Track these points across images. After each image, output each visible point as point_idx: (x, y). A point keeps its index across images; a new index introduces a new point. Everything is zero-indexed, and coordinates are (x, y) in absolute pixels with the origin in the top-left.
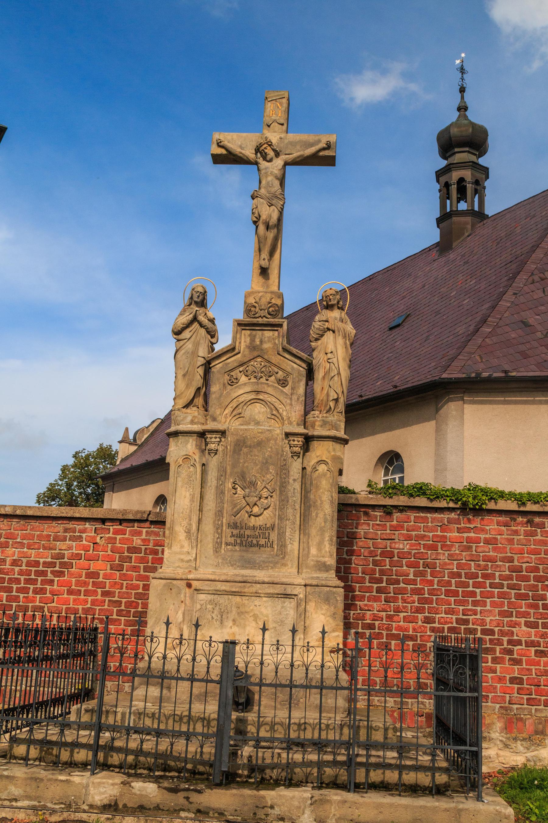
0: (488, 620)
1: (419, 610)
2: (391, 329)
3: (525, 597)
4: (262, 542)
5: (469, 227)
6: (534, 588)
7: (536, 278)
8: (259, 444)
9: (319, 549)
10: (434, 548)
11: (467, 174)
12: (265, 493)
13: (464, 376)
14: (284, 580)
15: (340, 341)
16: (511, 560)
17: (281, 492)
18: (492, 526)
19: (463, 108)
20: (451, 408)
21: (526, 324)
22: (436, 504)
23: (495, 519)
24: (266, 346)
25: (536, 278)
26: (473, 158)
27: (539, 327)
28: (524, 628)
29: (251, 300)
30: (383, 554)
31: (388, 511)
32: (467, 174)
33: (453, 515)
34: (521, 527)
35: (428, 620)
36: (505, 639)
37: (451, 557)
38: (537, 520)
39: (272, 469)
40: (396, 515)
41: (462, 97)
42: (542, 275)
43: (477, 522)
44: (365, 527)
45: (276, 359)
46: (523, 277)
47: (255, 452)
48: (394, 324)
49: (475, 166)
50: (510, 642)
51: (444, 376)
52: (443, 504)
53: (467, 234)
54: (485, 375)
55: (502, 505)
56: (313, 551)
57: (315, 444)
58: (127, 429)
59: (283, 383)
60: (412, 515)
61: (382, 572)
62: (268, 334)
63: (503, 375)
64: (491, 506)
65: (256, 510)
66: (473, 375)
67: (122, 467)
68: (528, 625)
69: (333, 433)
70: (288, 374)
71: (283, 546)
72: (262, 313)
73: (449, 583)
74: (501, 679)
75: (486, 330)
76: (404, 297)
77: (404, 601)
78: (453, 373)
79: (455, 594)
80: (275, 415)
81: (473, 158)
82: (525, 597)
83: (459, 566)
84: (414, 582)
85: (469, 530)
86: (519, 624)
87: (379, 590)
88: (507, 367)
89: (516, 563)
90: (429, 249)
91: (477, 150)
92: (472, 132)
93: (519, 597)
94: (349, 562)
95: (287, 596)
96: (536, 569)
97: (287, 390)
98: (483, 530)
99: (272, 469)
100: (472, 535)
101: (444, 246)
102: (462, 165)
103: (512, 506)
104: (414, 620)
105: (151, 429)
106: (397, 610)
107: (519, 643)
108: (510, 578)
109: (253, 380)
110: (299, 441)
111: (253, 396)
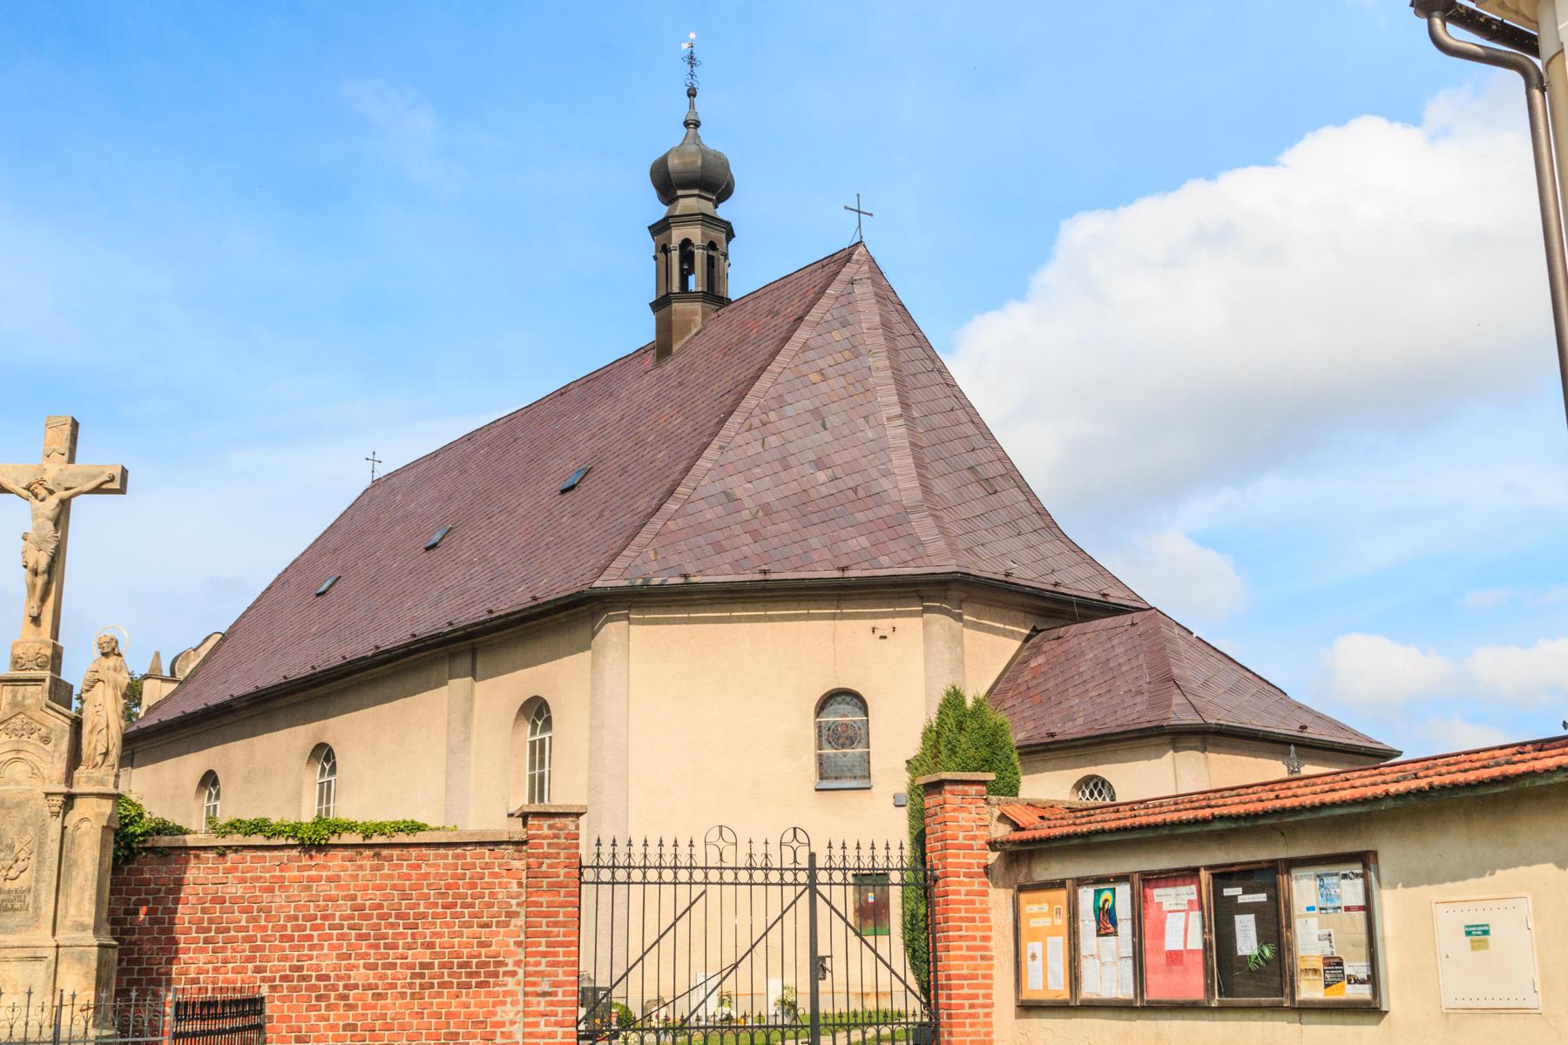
0: (324, 964)
1: (249, 960)
2: (563, 492)
3: (366, 937)
4: (17, 905)
5: (699, 319)
6: (377, 927)
7: (756, 422)
8: (19, 805)
9: (79, 909)
10: (270, 890)
11: (695, 233)
12: (22, 856)
13: (626, 583)
14: (36, 943)
15: (110, 692)
16: (354, 898)
17: (39, 853)
18: (336, 861)
19: (692, 124)
20: (612, 632)
21: (729, 497)
22: (274, 842)
23: (341, 853)
24: (28, 702)
25: (756, 422)
26: (707, 207)
27: (748, 503)
28: (362, 970)
29: (19, 651)
30: (213, 901)
31: (222, 852)
32: (695, 233)
33: (294, 853)
34: (367, 860)
35: (258, 970)
36: (341, 984)
37: (289, 900)
38: (385, 852)
39: (31, 830)
40: (231, 856)
41: (692, 105)
42: (764, 417)
43: (320, 858)
44: (195, 871)
45: (38, 715)
46: (735, 420)
47: (14, 812)
48: (567, 485)
49: (708, 220)
50: (346, 987)
51: (598, 584)
52: (281, 841)
53: (694, 331)
54: (656, 581)
55: (347, 838)
56: (72, 911)
57: (78, 801)
58: (157, 655)
59: (46, 740)
60: (248, 855)
61: (211, 921)
62: (31, 689)
63: (681, 580)
64: (334, 840)
65: (12, 873)
66: (639, 582)
67: (143, 725)
68: (368, 967)
69: (103, 790)
70: (51, 730)
71: (37, 909)
72: (29, 665)
73: (284, 928)
74: (333, 1028)
75: (671, 506)
76: (594, 435)
77: (234, 951)
78: (611, 580)
79: (291, 938)
80: (35, 773)
81: (707, 207)
82: (366, 937)
83: (296, 909)
84: (246, 929)
85: (310, 868)
86: (357, 967)
87: (206, 941)
88: (689, 569)
89: (359, 901)
90: (643, 351)
91: (713, 193)
92: (703, 166)
93: (360, 937)
94: (175, 911)
95: (37, 959)
96: (380, 906)
97: (49, 747)
98: (326, 868)
99: (31, 830)
100: (313, 873)
101: (662, 348)
102: (687, 219)
103: (356, 838)
104: (242, 970)
105: (203, 652)
106: (225, 961)
107: (356, 987)
108: (351, 917)
109: (14, 738)
110: (59, 800)
111: (13, 755)
